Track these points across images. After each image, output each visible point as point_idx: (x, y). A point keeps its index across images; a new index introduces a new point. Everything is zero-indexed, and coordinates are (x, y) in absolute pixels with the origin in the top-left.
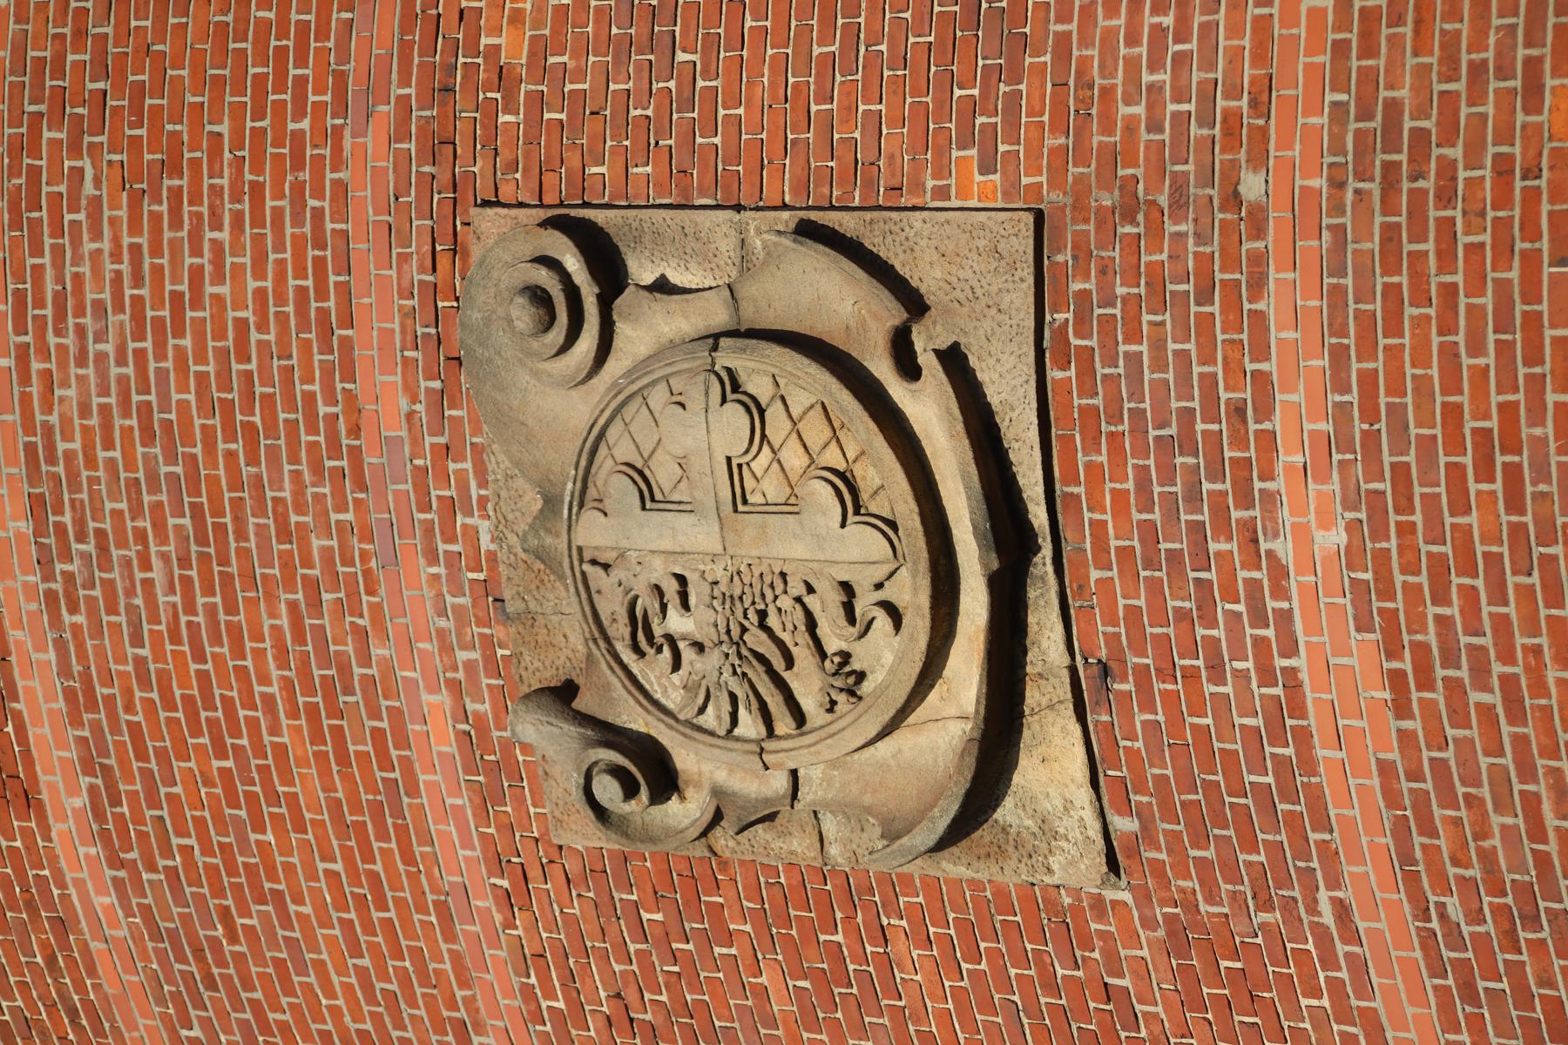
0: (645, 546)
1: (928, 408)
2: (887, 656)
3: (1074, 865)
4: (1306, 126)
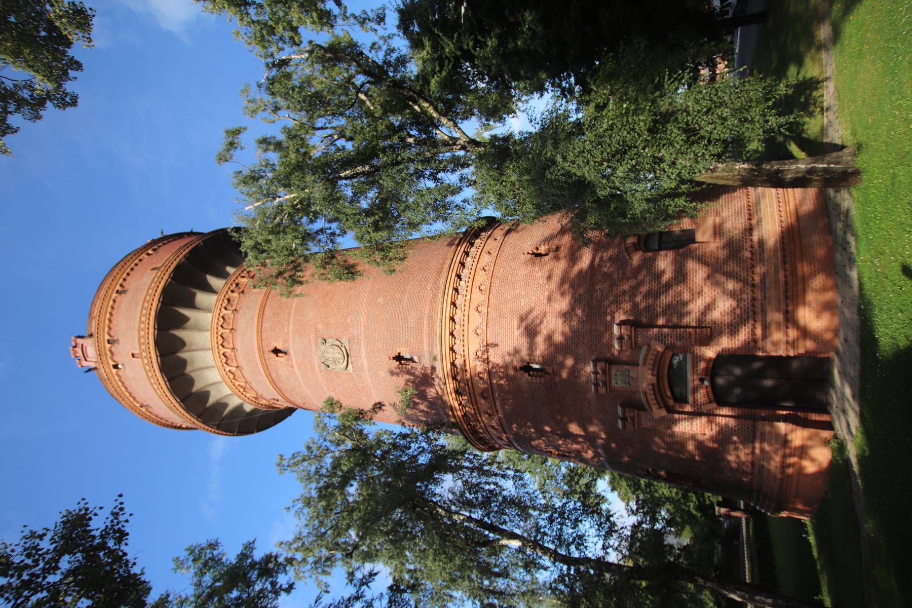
0: (328, 356)
1: (343, 349)
2: (341, 361)
4: (363, 335)
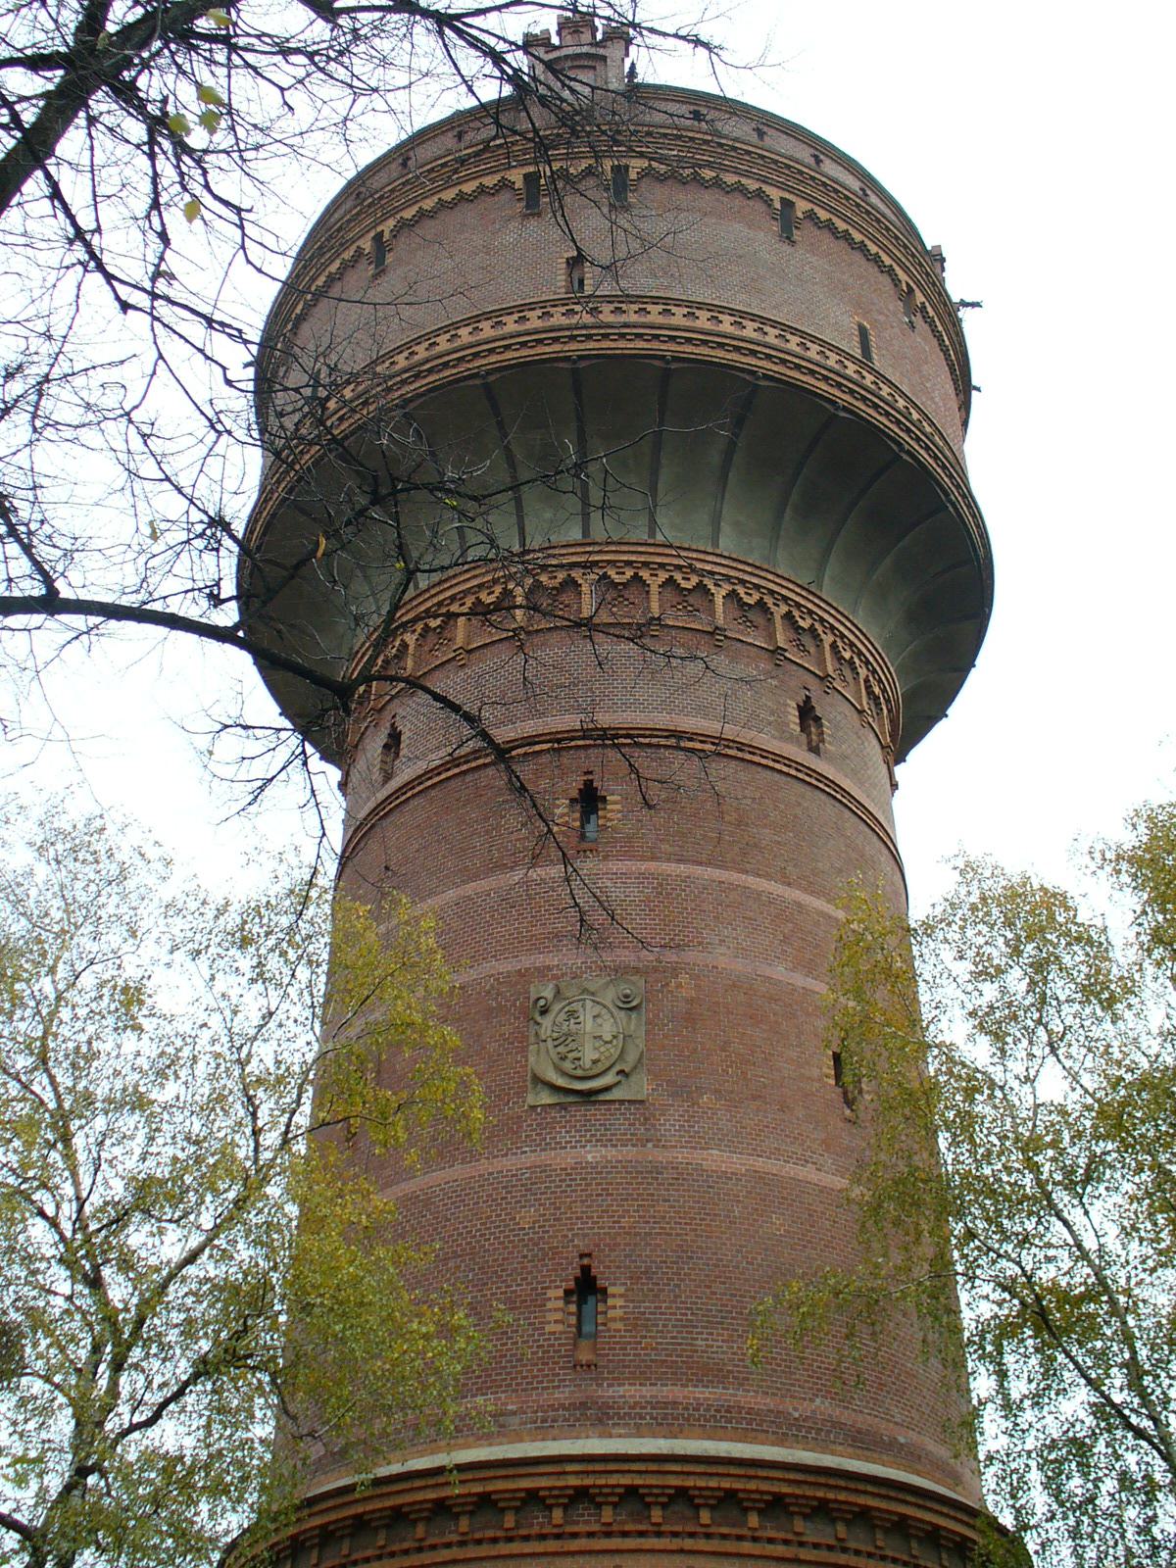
1: (609, 1079)
3: (531, 1100)
